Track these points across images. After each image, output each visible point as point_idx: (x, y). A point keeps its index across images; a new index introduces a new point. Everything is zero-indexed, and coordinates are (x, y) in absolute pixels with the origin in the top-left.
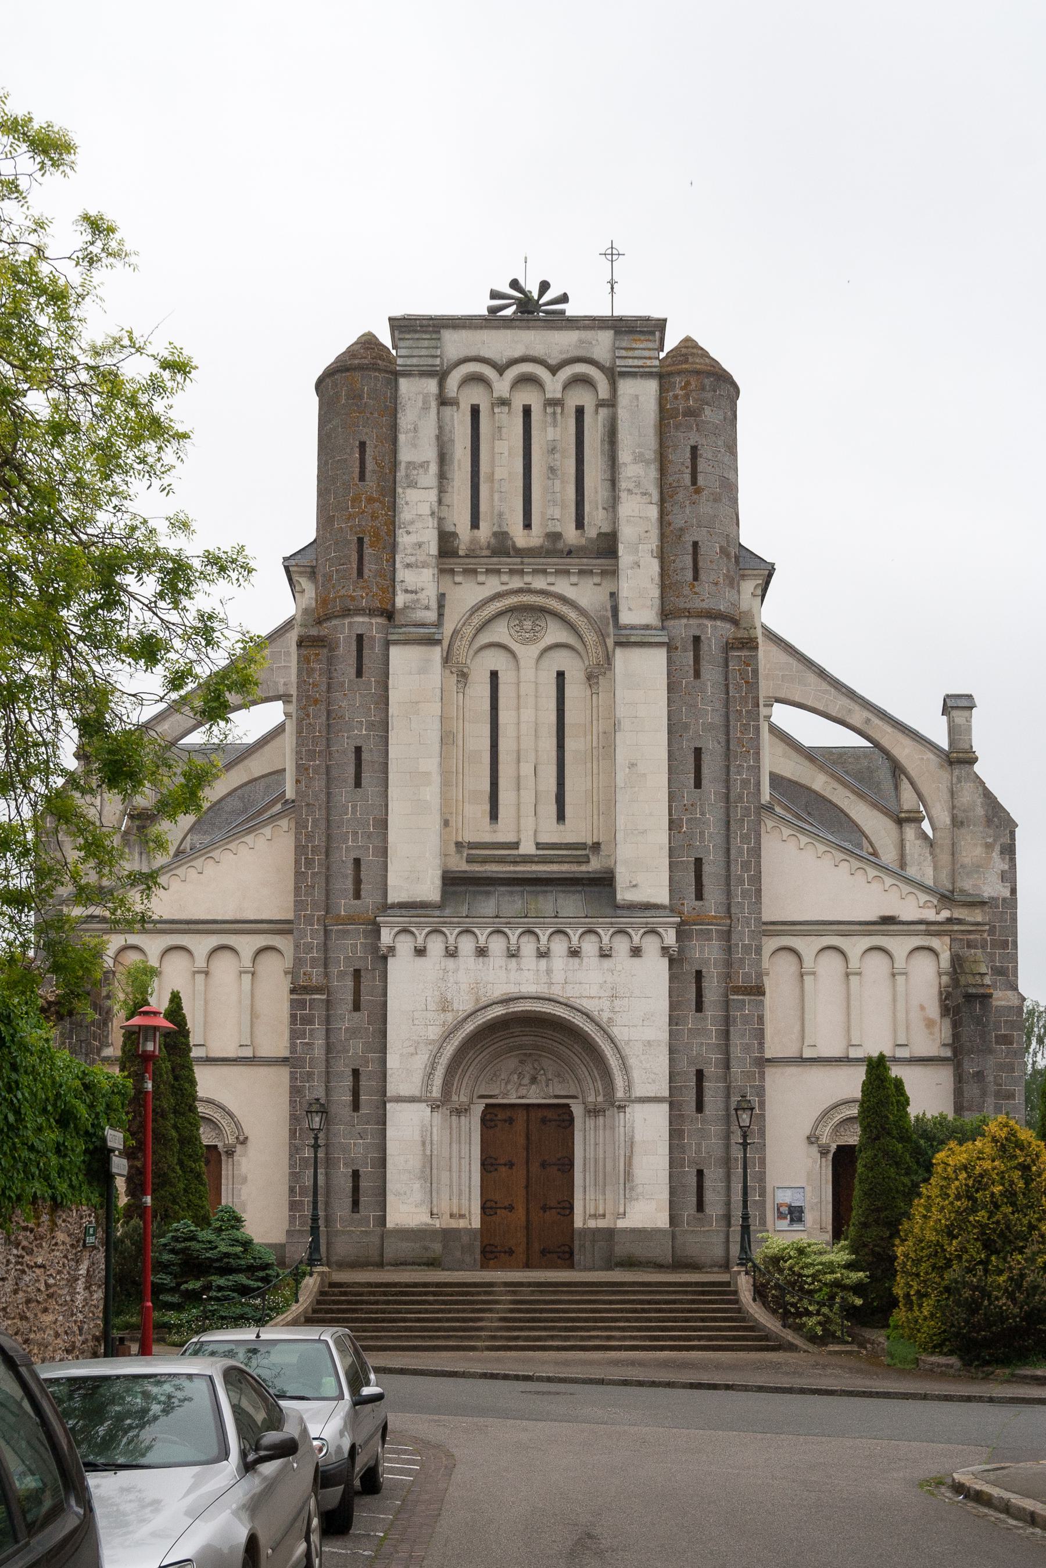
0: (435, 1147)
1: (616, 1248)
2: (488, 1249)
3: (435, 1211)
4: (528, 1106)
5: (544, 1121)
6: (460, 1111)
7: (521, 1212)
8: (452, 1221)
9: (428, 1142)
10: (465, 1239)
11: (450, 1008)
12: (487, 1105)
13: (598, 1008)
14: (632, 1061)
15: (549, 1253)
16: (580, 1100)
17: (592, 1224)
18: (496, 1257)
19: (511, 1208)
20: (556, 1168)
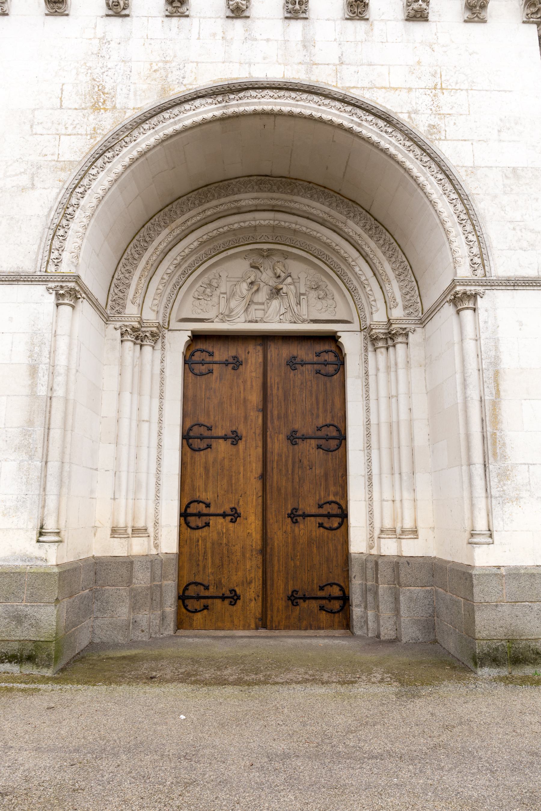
0: (60, 379)
1: (479, 617)
2: (192, 591)
3: (50, 526)
4: (265, 339)
5: (293, 363)
7: (252, 523)
9: (43, 369)
10: (142, 579)
11: (109, 105)
12: (197, 337)
14: (482, 206)
15: (304, 598)
16: (356, 326)
17: (389, 548)
18: (206, 607)
19: (234, 515)
20: (313, 442)
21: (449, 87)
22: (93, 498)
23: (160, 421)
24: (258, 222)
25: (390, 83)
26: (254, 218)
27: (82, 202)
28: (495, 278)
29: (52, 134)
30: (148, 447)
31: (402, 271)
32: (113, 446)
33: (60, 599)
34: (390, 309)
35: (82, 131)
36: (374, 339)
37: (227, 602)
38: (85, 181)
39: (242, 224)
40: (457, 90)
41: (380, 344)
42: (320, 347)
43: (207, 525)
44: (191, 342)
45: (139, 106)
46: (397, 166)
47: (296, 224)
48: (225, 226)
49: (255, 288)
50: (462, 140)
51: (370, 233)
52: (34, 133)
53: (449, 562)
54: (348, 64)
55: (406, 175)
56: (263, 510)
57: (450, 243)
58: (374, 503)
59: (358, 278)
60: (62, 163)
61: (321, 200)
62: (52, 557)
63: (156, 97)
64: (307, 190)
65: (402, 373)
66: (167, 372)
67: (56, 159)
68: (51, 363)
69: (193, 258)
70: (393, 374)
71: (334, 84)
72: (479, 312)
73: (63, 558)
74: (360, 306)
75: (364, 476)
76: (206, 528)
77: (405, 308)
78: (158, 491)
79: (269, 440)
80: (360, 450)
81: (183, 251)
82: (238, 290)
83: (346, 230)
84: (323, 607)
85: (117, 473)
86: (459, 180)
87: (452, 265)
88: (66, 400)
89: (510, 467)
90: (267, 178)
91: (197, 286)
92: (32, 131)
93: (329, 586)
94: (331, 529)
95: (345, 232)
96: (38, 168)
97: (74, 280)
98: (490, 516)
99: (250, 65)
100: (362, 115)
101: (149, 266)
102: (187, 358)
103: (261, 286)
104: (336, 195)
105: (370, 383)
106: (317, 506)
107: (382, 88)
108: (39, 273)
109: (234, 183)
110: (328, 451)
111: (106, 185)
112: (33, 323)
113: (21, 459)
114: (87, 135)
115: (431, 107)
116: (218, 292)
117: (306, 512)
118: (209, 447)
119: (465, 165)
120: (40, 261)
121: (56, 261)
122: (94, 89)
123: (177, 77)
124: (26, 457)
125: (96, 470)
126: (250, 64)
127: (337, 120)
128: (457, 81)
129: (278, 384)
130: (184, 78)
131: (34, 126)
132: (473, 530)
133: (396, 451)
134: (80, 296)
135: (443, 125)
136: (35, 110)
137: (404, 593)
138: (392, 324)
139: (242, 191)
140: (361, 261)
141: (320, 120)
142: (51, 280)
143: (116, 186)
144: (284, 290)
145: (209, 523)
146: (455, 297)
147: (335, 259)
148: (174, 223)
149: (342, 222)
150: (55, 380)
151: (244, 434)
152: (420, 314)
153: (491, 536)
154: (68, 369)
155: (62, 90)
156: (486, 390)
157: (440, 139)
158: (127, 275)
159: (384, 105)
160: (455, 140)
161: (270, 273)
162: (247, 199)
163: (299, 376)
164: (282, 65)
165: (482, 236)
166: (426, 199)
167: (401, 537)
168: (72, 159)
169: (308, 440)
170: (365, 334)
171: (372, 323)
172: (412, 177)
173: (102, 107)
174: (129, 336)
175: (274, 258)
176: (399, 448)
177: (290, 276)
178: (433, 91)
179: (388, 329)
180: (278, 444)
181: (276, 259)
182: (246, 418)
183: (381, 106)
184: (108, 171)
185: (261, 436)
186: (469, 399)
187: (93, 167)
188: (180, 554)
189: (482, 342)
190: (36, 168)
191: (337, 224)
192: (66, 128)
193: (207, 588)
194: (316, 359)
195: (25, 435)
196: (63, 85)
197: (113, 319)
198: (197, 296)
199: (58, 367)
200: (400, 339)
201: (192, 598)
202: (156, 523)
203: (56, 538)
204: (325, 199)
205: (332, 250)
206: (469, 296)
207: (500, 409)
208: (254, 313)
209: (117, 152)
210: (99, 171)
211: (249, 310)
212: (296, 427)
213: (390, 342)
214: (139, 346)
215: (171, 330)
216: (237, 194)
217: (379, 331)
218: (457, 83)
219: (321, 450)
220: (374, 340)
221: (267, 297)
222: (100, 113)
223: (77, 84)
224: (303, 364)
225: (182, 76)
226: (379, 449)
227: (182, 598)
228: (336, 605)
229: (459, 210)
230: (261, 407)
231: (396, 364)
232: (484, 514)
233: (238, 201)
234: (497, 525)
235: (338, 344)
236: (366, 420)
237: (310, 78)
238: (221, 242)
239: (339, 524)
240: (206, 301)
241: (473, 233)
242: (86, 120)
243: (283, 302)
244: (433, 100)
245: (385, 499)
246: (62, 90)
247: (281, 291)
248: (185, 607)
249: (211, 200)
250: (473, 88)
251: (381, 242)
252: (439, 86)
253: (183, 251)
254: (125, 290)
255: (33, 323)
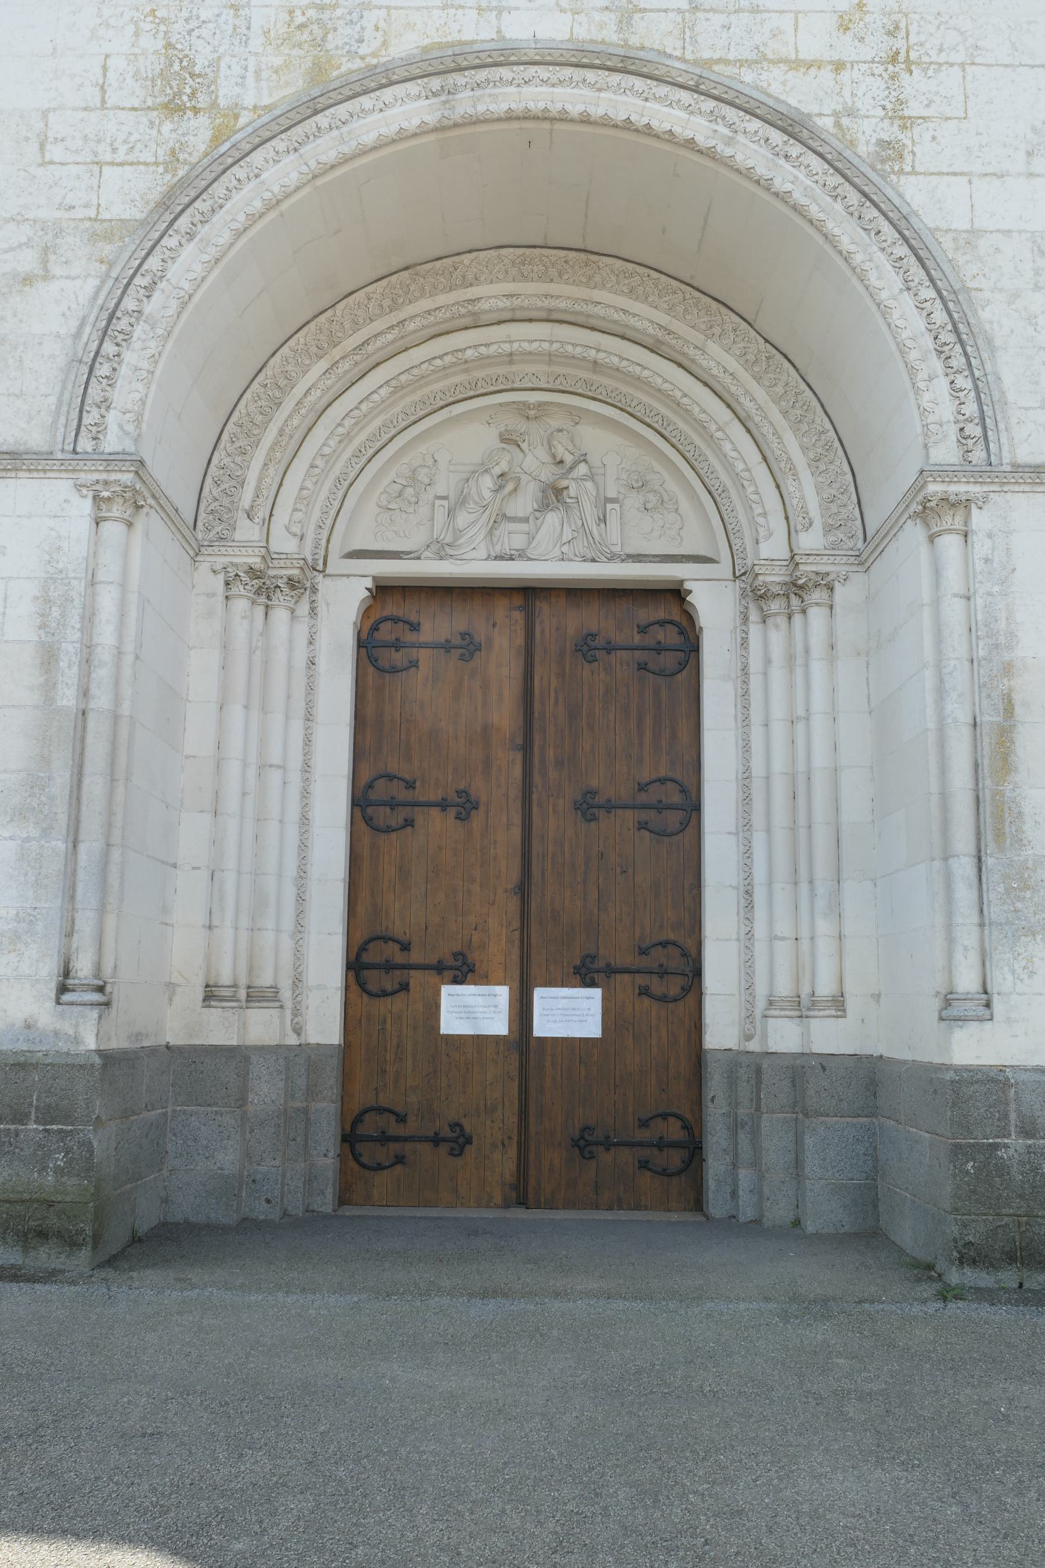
0: (102, 674)
2: (369, 1126)
3: (83, 967)
4: (529, 594)
6: (268, 585)
8: (214, 1015)
10: (266, 1091)
13: (833, 105)
14: (994, 316)
16: (724, 568)
17: (784, 1037)
18: (400, 1160)
21: (925, 59)
22: (166, 924)
23: (307, 767)
24: (516, 345)
25: (797, 51)
26: (509, 336)
27: (148, 308)
28: (1009, 469)
29: (85, 163)
30: (281, 821)
31: (823, 452)
32: (208, 817)
33: (104, 1118)
34: (796, 531)
35: (147, 156)
36: (761, 597)
37: (444, 1148)
38: (153, 263)
39: (483, 350)
40: (940, 65)
41: (775, 606)
42: (646, 614)
43: (405, 987)
44: (371, 602)
45: (266, 101)
46: (810, 230)
47: (598, 351)
48: (447, 354)
49: (510, 487)
50: (948, 174)
51: (755, 369)
52: (46, 160)
53: (905, 1062)
54: (708, 11)
55: (828, 248)
56: (522, 958)
57: (916, 393)
58: (756, 944)
59: (729, 467)
60: (105, 225)
61: (650, 299)
62: (87, 1034)
63: (301, 82)
64: (621, 276)
65: (818, 668)
66: (323, 664)
67: (93, 216)
68: (84, 641)
69: (378, 422)
70: (799, 671)
71: (678, 53)
72: (975, 539)
73: (109, 1039)
74: (733, 526)
75: (737, 888)
76: (402, 994)
77: (828, 530)
78: (300, 913)
79: (535, 810)
80: (729, 833)
81: (356, 408)
82: (474, 491)
83: (705, 363)
84: (647, 1162)
85: (215, 873)
86: (938, 260)
87: (921, 439)
88: (116, 718)
89: (1030, 862)
90: (537, 251)
91: (386, 481)
92: (43, 157)
93: (660, 1120)
94: (663, 999)
95: (701, 367)
96: (56, 236)
97: (132, 468)
98: (988, 964)
99: (500, 13)
100: (736, 120)
101: (285, 438)
102: (364, 636)
103: (523, 482)
104: (684, 287)
105: (752, 691)
106: (637, 950)
107: (781, 61)
108: (59, 456)
109: (467, 262)
110: (662, 833)
111: (198, 269)
112: (47, 557)
113: (25, 835)
114: (157, 164)
115: (883, 103)
116: (427, 497)
117: (613, 964)
118: (409, 823)
119: (953, 227)
120: (63, 430)
121: (94, 429)
122: (171, 65)
123: (346, 40)
124: (34, 832)
125: (175, 866)
126: (500, 11)
127: (684, 132)
128: (942, 45)
129: (556, 692)
130: (361, 41)
131: (48, 147)
132: (951, 993)
133: (802, 832)
134: (142, 503)
135: (908, 142)
136: (48, 110)
137: (814, 1130)
138: (797, 564)
139: (482, 279)
140: (737, 430)
141: (648, 131)
142: (86, 468)
143: (216, 272)
144: (572, 492)
145: (408, 984)
146: (925, 508)
147: (681, 425)
148: (338, 348)
149: (696, 347)
150: (94, 675)
151: (483, 798)
152: (860, 544)
153: (988, 1005)
154: (119, 653)
155: (105, 69)
156: (985, 702)
157: (901, 171)
158: (239, 459)
159: (783, 97)
160: (932, 174)
161: (542, 454)
162: (492, 294)
163: (602, 675)
164: (569, 13)
165: (984, 379)
166: (868, 300)
167: (811, 1013)
168: (126, 216)
169: (620, 812)
170: (743, 585)
171: (756, 562)
172: (840, 253)
173: (188, 104)
174: (241, 588)
175: (551, 422)
176: (810, 827)
177: (585, 461)
178: (891, 67)
179: (791, 575)
180: (556, 822)
181: (554, 423)
182: (487, 763)
183: (777, 99)
184: (201, 240)
185: (519, 803)
186: (950, 721)
187: (171, 232)
188: (347, 1047)
189: (979, 602)
190: (51, 235)
191: (685, 349)
192: (114, 150)
193: (401, 1119)
194: (637, 639)
195: (32, 787)
196: (107, 56)
197: (210, 550)
198: (385, 503)
199: (99, 650)
200: (817, 596)
201: (371, 1139)
202: (297, 981)
203: (96, 997)
204: (660, 297)
205: (675, 406)
206: (953, 505)
207: (1013, 743)
208: (506, 540)
209: (221, 201)
210: (183, 241)
211: (497, 533)
212: (594, 783)
213: (795, 601)
214: (262, 609)
215: (329, 575)
216: (471, 285)
217: (774, 578)
218: (941, 50)
219: (647, 833)
220: (760, 596)
221: (536, 506)
222: (185, 118)
223: (136, 55)
224: (610, 648)
225: (357, 37)
226: (768, 830)
227: (350, 1139)
228: (675, 1159)
229: (938, 323)
230: (520, 741)
231: (807, 651)
232: (974, 958)
233: (473, 301)
234: (1001, 980)
235: (685, 607)
236: (741, 769)
237: (626, 40)
238: (436, 387)
239: (683, 989)
240: (404, 515)
241: (966, 373)
242: (154, 132)
243: (568, 517)
244: (888, 88)
245: (780, 934)
246: (105, 69)
247: (565, 493)
248: (356, 1158)
249: (417, 299)
250: (977, 60)
251: (779, 389)
252: (902, 57)
253: (356, 408)
254: (233, 489)
255: (47, 557)
